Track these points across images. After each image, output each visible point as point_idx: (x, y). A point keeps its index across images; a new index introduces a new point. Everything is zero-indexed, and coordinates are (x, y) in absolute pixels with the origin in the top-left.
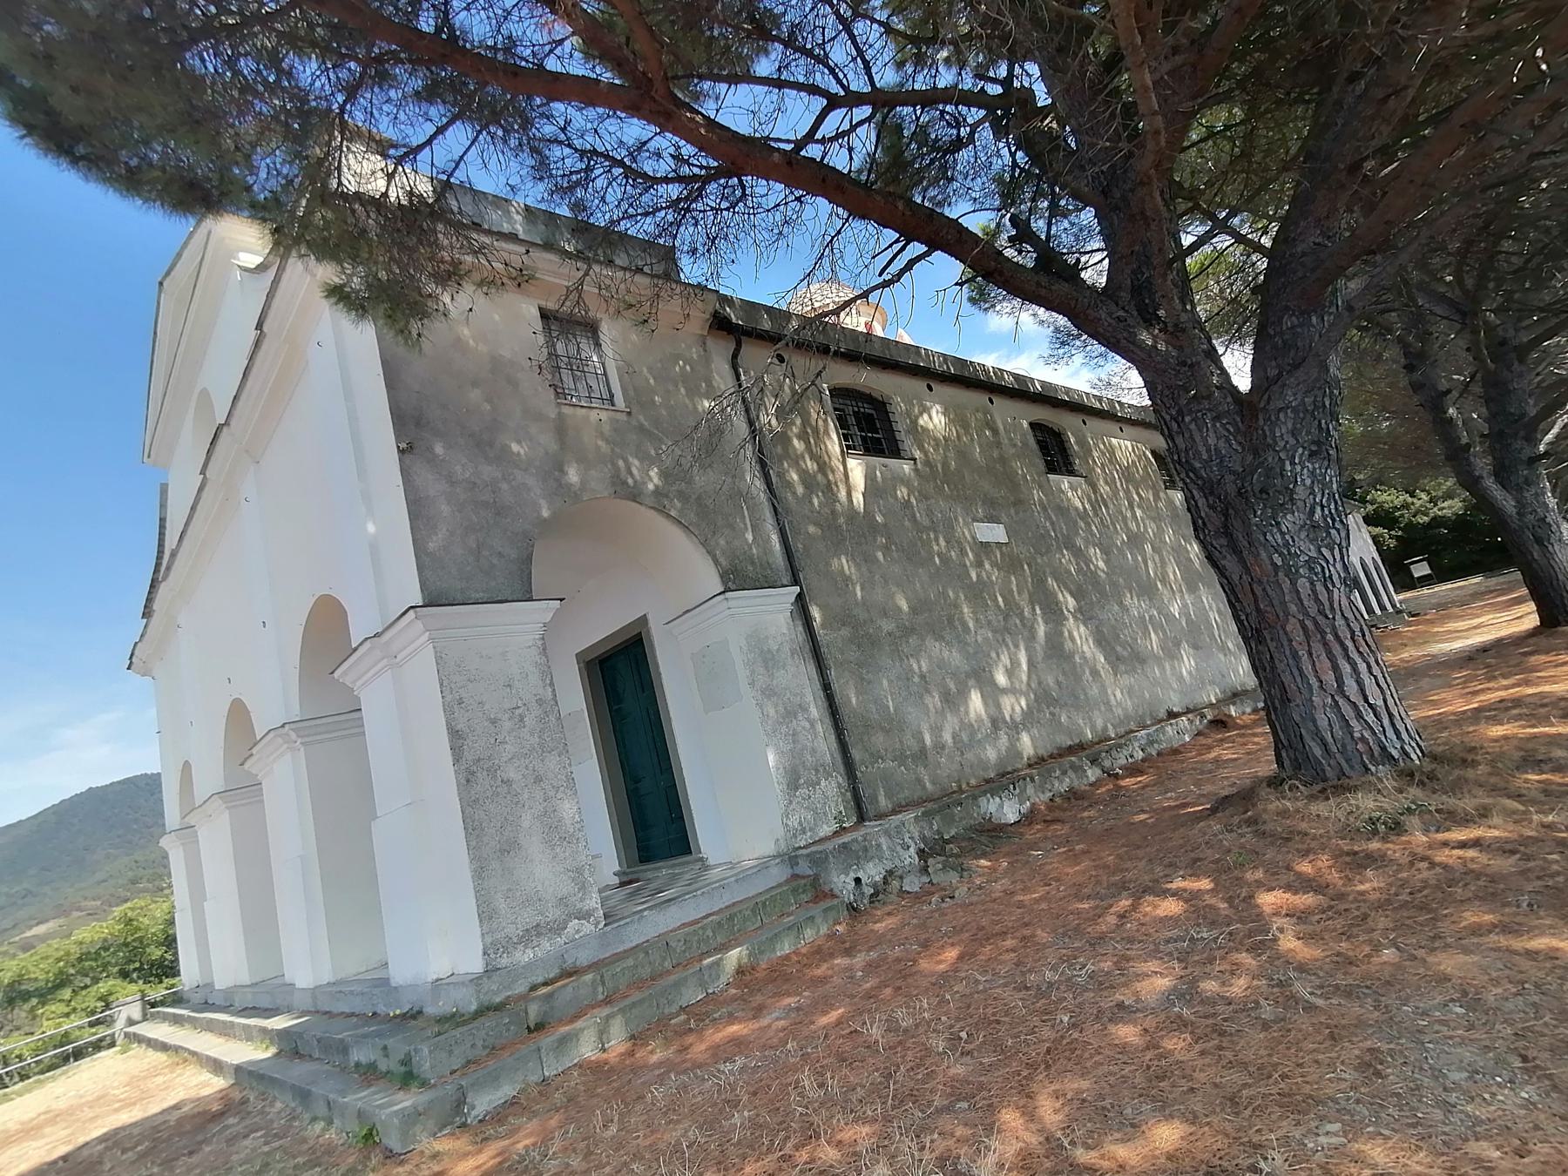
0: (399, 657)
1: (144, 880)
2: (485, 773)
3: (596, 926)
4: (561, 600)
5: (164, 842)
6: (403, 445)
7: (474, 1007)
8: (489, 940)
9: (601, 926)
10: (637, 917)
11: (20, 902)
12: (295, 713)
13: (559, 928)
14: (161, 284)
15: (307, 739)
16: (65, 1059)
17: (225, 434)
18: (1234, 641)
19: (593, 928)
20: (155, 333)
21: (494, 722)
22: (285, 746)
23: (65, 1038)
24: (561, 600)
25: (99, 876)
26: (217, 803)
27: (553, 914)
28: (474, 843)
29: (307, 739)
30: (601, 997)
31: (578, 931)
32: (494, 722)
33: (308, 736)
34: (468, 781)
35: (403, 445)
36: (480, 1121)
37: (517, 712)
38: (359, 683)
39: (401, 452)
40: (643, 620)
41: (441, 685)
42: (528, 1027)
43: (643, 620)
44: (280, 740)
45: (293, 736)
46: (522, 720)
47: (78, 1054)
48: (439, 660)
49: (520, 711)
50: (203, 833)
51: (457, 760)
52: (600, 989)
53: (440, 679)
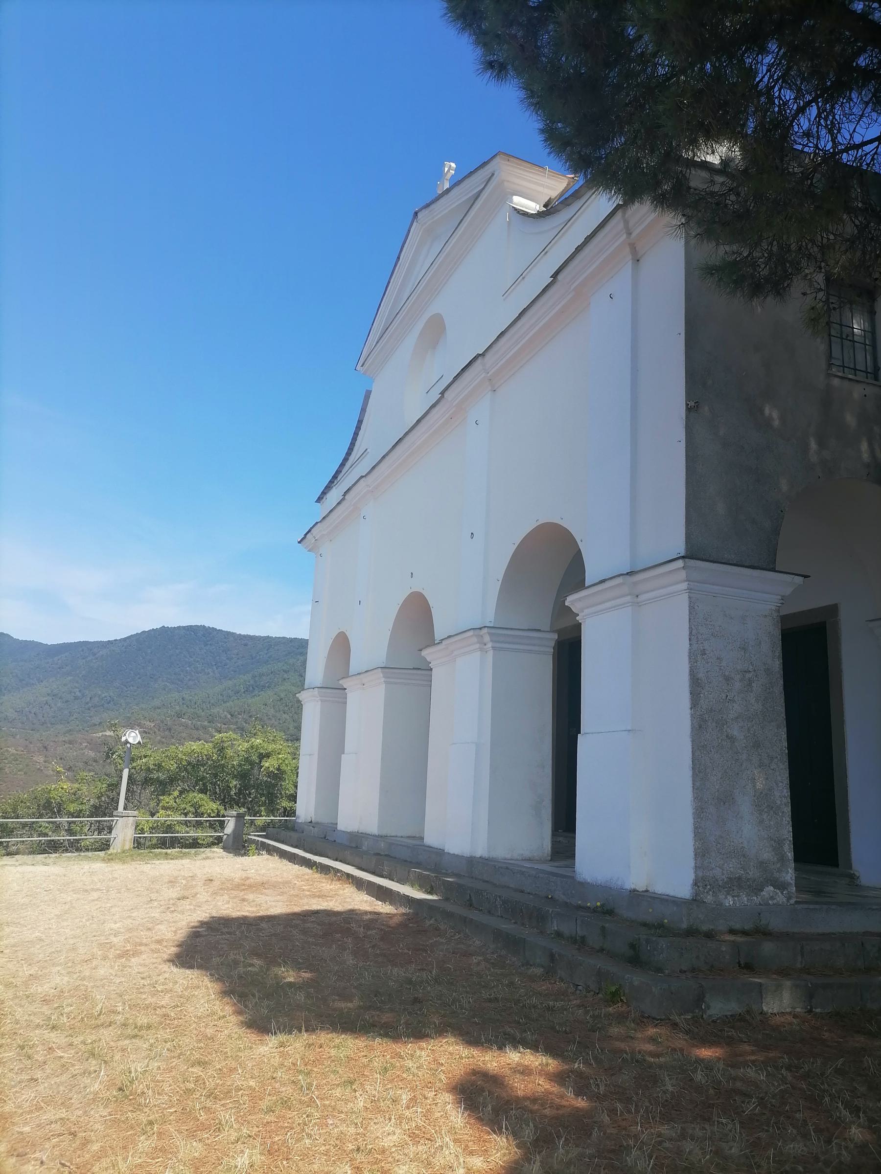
0: (642, 598)
1: (186, 717)
2: (714, 724)
3: (789, 898)
4: (806, 577)
5: (302, 696)
6: (692, 404)
7: (684, 926)
8: (700, 874)
9: (792, 901)
10: (825, 907)
11: (106, 705)
12: (490, 618)
13: (757, 889)
14: (416, 214)
15: (498, 645)
16: (163, 844)
17: (479, 360)
18: (191, 850)
19: (785, 900)
20: (399, 258)
21: (727, 679)
22: (477, 646)
23: (169, 828)
24: (806, 577)
25: (157, 702)
26: (379, 674)
27: (753, 873)
28: (698, 784)
29: (498, 645)
30: (799, 965)
31: (772, 898)
32: (727, 679)
33: (499, 642)
34: (700, 727)
35: (692, 404)
36: (713, 1021)
37: (748, 676)
38: (586, 611)
39: (689, 409)
40: (833, 610)
41: (691, 633)
42: (739, 963)
43: (833, 610)
44: (475, 639)
45: (487, 638)
46: (750, 685)
47: (173, 843)
48: (692, 608)
49: (750, 675)
50: (353, 699)
51: (694, 704)
52: (799, 958)
53: (690, 628)
